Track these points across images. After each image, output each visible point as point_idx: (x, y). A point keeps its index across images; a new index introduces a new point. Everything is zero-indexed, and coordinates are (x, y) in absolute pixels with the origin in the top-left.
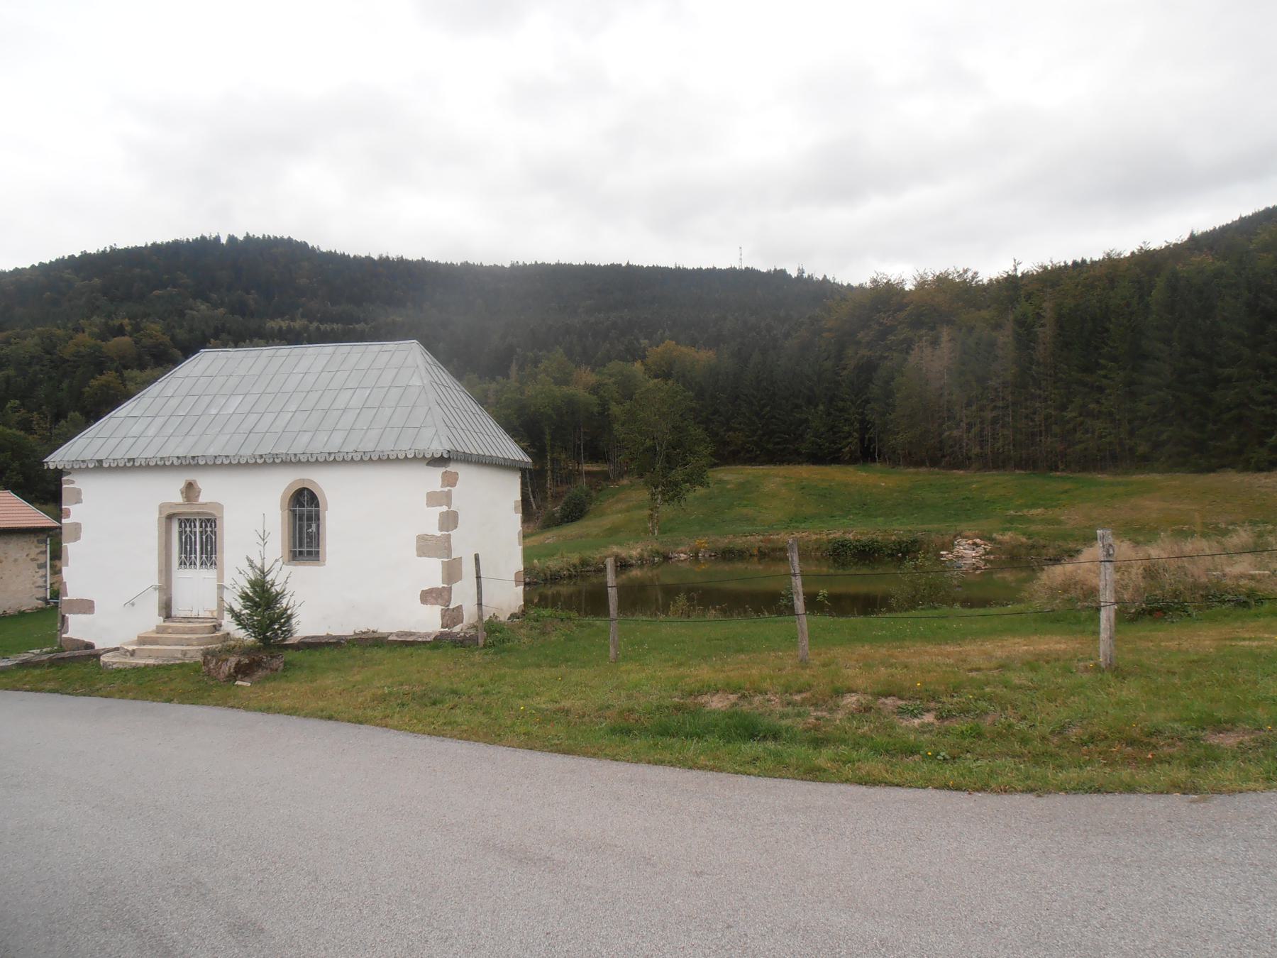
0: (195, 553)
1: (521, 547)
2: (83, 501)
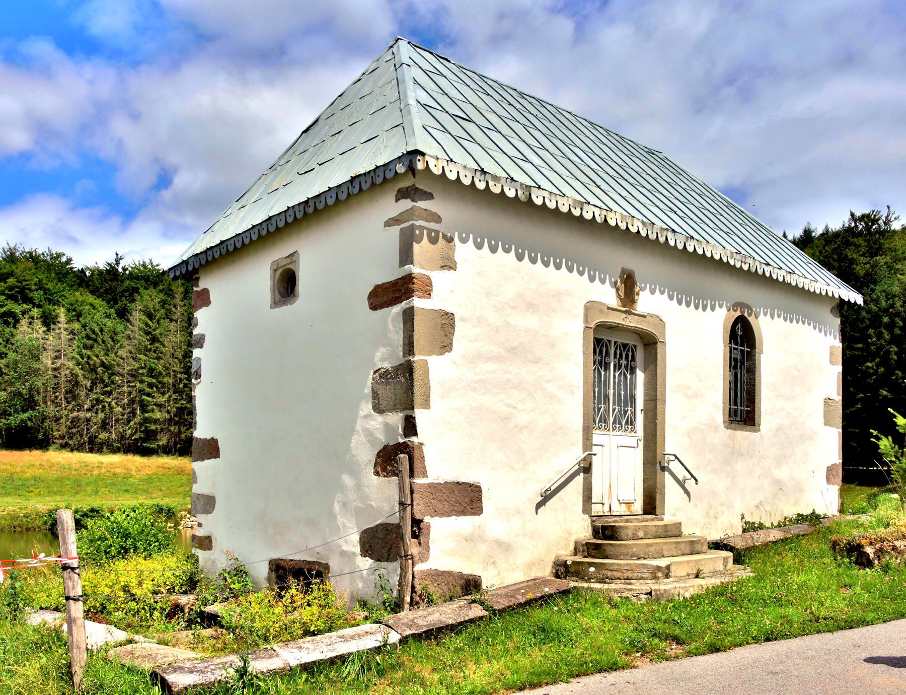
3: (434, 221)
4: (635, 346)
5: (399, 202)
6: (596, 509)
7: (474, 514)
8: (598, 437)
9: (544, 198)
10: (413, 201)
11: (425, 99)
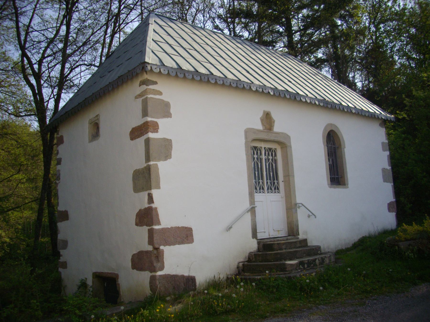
0: (262, 179)
1: (388, 153)
2: (61, 157)
3: (158, 94)
4: (276, 149)
5: (141, 87)
6: (260, 236)
7: (189, 243)
8: (258, 197)
9: (216, 79)
10: (147, 86)
11: (158, 38)
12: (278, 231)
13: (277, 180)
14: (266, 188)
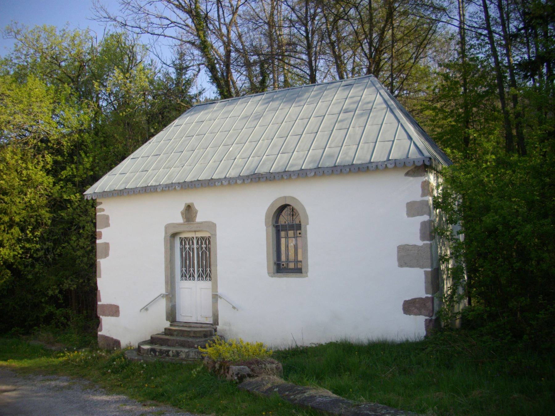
0: (194, 267)
12: (207, 317)
13: (210, 267)
14: (196, 276)
